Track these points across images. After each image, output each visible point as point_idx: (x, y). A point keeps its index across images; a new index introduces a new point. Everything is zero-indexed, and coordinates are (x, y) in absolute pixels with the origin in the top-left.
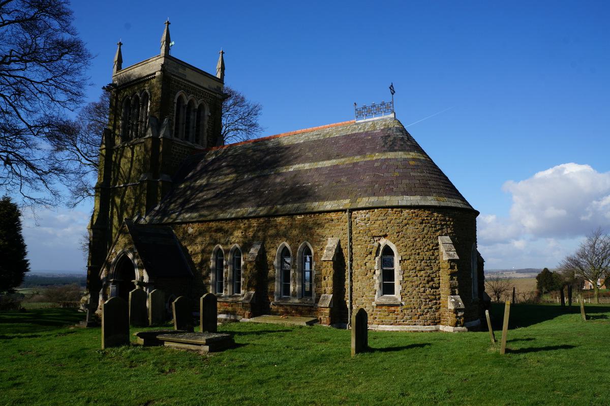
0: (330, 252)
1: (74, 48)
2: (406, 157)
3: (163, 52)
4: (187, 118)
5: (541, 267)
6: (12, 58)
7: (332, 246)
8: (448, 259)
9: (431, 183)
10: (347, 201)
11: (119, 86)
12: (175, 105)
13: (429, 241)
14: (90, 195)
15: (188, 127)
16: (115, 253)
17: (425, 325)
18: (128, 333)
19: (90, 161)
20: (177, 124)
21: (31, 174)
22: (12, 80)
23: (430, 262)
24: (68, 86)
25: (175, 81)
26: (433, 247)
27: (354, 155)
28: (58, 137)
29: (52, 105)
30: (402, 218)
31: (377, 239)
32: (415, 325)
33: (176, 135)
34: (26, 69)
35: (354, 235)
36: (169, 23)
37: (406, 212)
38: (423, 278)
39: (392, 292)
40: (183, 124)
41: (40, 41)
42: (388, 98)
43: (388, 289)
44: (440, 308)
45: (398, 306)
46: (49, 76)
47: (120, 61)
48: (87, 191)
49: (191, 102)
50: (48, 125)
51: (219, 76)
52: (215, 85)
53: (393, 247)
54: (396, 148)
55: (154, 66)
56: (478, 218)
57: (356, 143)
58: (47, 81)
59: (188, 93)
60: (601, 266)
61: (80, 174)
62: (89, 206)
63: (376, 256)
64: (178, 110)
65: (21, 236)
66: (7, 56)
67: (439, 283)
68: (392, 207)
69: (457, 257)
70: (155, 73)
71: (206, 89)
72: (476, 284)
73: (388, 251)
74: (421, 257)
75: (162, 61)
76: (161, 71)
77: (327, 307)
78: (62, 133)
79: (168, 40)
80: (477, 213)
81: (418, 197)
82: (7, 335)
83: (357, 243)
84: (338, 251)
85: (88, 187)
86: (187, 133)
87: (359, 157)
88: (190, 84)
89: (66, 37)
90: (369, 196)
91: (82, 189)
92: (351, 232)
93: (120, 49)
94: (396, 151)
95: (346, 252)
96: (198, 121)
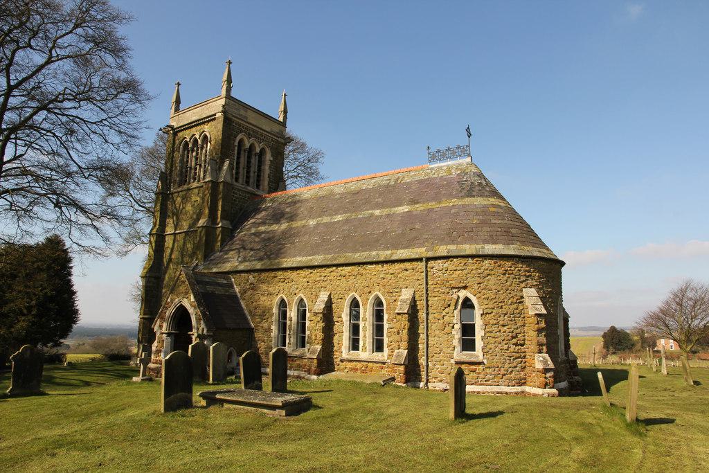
0: (405, 305)
1: (130, 87)
2: (485, 203)
3: (224, 93)
4: (248, 162)
5: (607, 326)
6: (66, 96)
7: (406, 297)
8: (534, 313)
9: (513, 231)
10: (423, 250)
11: (176, 128)
12: (236, 148)
13: (513, 293)
14: (143, 243)
15: (248, 172)
16: (172, 303)
17: (509, 386)
18: (191, 392)
19: (143, 207)
20: (238, 168)
21: (82, 219)
22: (64, 119)
23: (514, 317)
24: (123, 128)
25: (236, 124)
26: (517, 300)
27: (427, 201)
28: (110, 183)
29: (106, 146)
30: (483, 268)
31: (456, 290)
32: (498, 385)
33: (237, 180)
34: (79, 107)
35: (431, 287)
36: (230, 62)
37: (487, 262)
38: (507, 334)
39: (473, 349)
40: (244, 169)
41: (96, 80)
42: (463, 140)
43: (468, 345)
44: (525, 367)
45: (479, 363)
46: (104, 116)
47: (178, 101)
48: (139, 239)
49: (252, 147)
50: (100, 168)
51: (281, 119)
52: (276, 129)
53: (474, 300)
54: (474, 193)
55: (216, 107)
56: (563, 270)
57: (429, 189)
58: (101, 122)
59: (249, 136)
60: (690, 325)
61: (133, 221)
62: (141, 254)
63: (455, 309)
64: (239, 153)
65: (70, 281)
66: (60, 94)
67: (524, 340)
68: (473, 257)
69: (544, 312)
70: (215, 115)
71: (267, 132)
73: (467, 304)
74: (504, 311)
75: (223, 102)
76: (222, 111)
77: (401, 365)
78: (114, 177)
79: (229, 80)
80: (562, 264)
81: (501, 246)
82: (185, 160)
83: (434, 295)
84: (413, 304)
85: (141, 234)
86: (248, 177)
87: (434, 203)
88: (251, 126)
89: (123, 75)
90: (447, 244)
91: (135, 237)
92: (427, 284)
93: (178, 89)
94: (474, 196)
95: (421, 305)
96: (259, 166)
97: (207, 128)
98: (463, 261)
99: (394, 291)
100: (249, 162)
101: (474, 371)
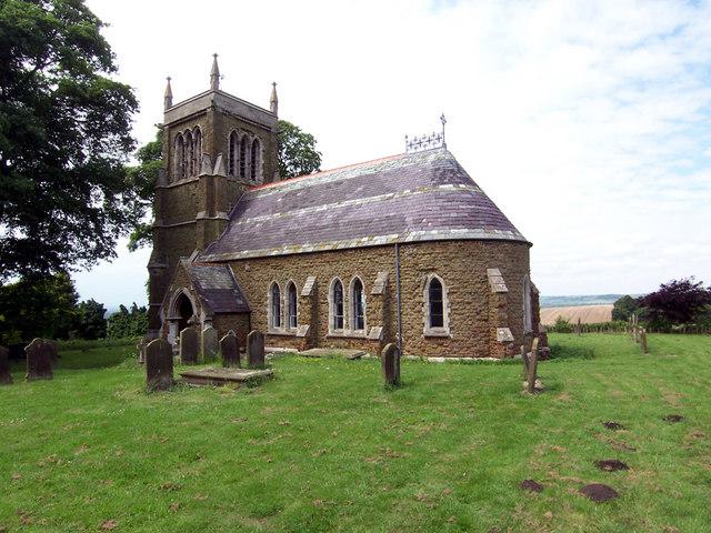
15: (242, 164)
16: (175, 291)
43: (437, 321)
64: (232, 146)
72: (529, 316)
80: (530, 245)
86: (243, 169)
95: (395, 286)
97: (200, 124)
98: (431, 245)
99: (371, 275)
100: (243, 155)
101: (441, 345)
